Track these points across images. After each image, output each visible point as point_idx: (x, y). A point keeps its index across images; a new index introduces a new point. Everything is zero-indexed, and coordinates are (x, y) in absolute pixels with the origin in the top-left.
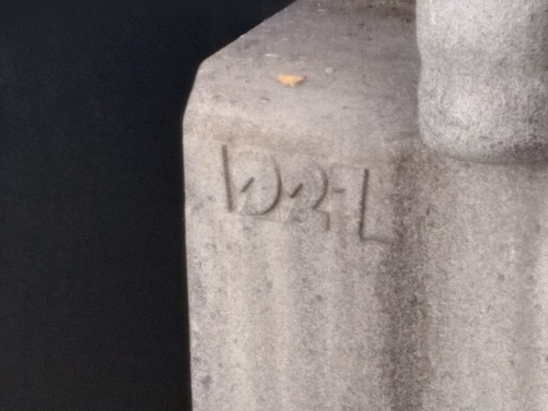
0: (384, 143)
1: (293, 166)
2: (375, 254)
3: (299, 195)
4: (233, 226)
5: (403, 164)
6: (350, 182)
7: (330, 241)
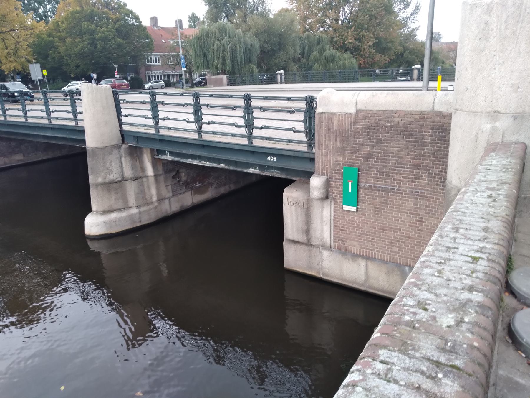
0: (306, 198)
1: (295, 200)
2: (305, 210)
3: (296, 203)
4: (289, 206)
5: (308, 200)
6: (302, 202)
7: (300, 208)
